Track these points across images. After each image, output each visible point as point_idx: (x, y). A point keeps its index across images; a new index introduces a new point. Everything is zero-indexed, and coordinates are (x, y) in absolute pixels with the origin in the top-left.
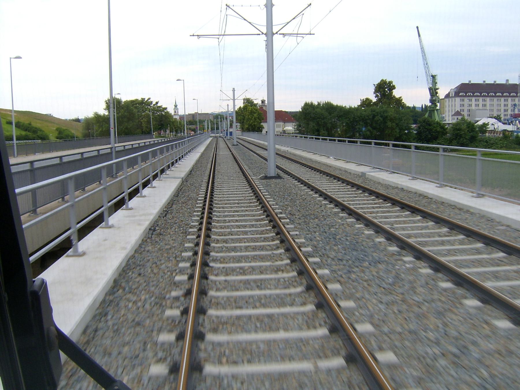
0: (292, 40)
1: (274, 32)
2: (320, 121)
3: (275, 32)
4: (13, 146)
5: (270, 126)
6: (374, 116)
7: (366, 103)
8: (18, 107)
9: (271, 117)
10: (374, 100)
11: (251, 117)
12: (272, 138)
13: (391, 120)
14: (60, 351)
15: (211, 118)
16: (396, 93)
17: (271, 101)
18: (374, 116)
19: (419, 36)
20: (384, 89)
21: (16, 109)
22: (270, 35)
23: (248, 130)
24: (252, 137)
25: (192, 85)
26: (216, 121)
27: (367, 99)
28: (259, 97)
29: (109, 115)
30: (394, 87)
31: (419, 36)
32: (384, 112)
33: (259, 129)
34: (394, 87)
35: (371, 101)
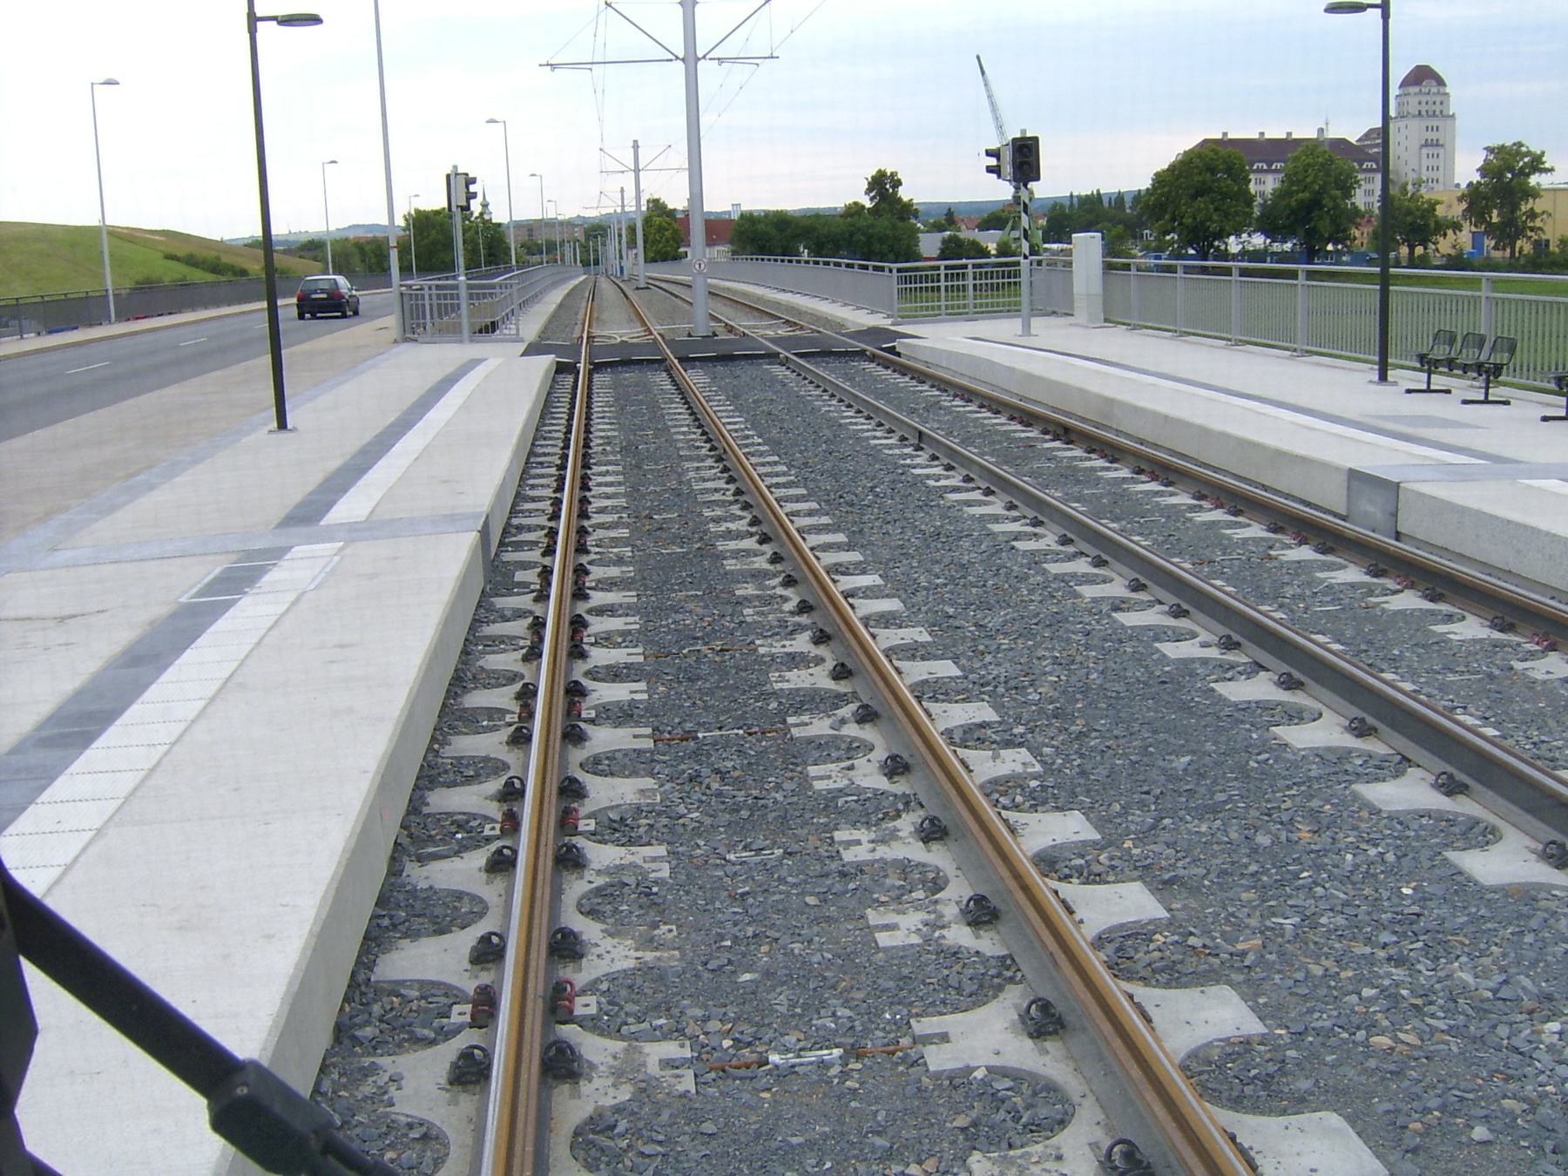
0: (739, 72)
1: (700, 55)
2: (767, 237)
3: (700, 55)
4: (106, 296)
5: (698, 251)
6: (851, 235)
7: (855, 210)
8: (124, 216)
9: (697, 232)
10: (868, 204)
11: (663, 233)
12: (703, 259)
13: (881, 240)
14: (33, 975)
15: (579, 234)
16: (904, 194)
17: (696, 191)
18: (851, 235)
19: (983, 73)
20: (883, 185)
21: (114, 220)
22: (691, 60)
23: (654, 260)
24: (661, 271)
25: (548, 175)
26: (590, 240)
27: (856, 204)
28: (677, 200)
29: (919, 258)
30: (899, 183)
31: (983, 73)
32: (868, 227)
33: (677, 257)
34: (899, 183)
35: (863, 207)
